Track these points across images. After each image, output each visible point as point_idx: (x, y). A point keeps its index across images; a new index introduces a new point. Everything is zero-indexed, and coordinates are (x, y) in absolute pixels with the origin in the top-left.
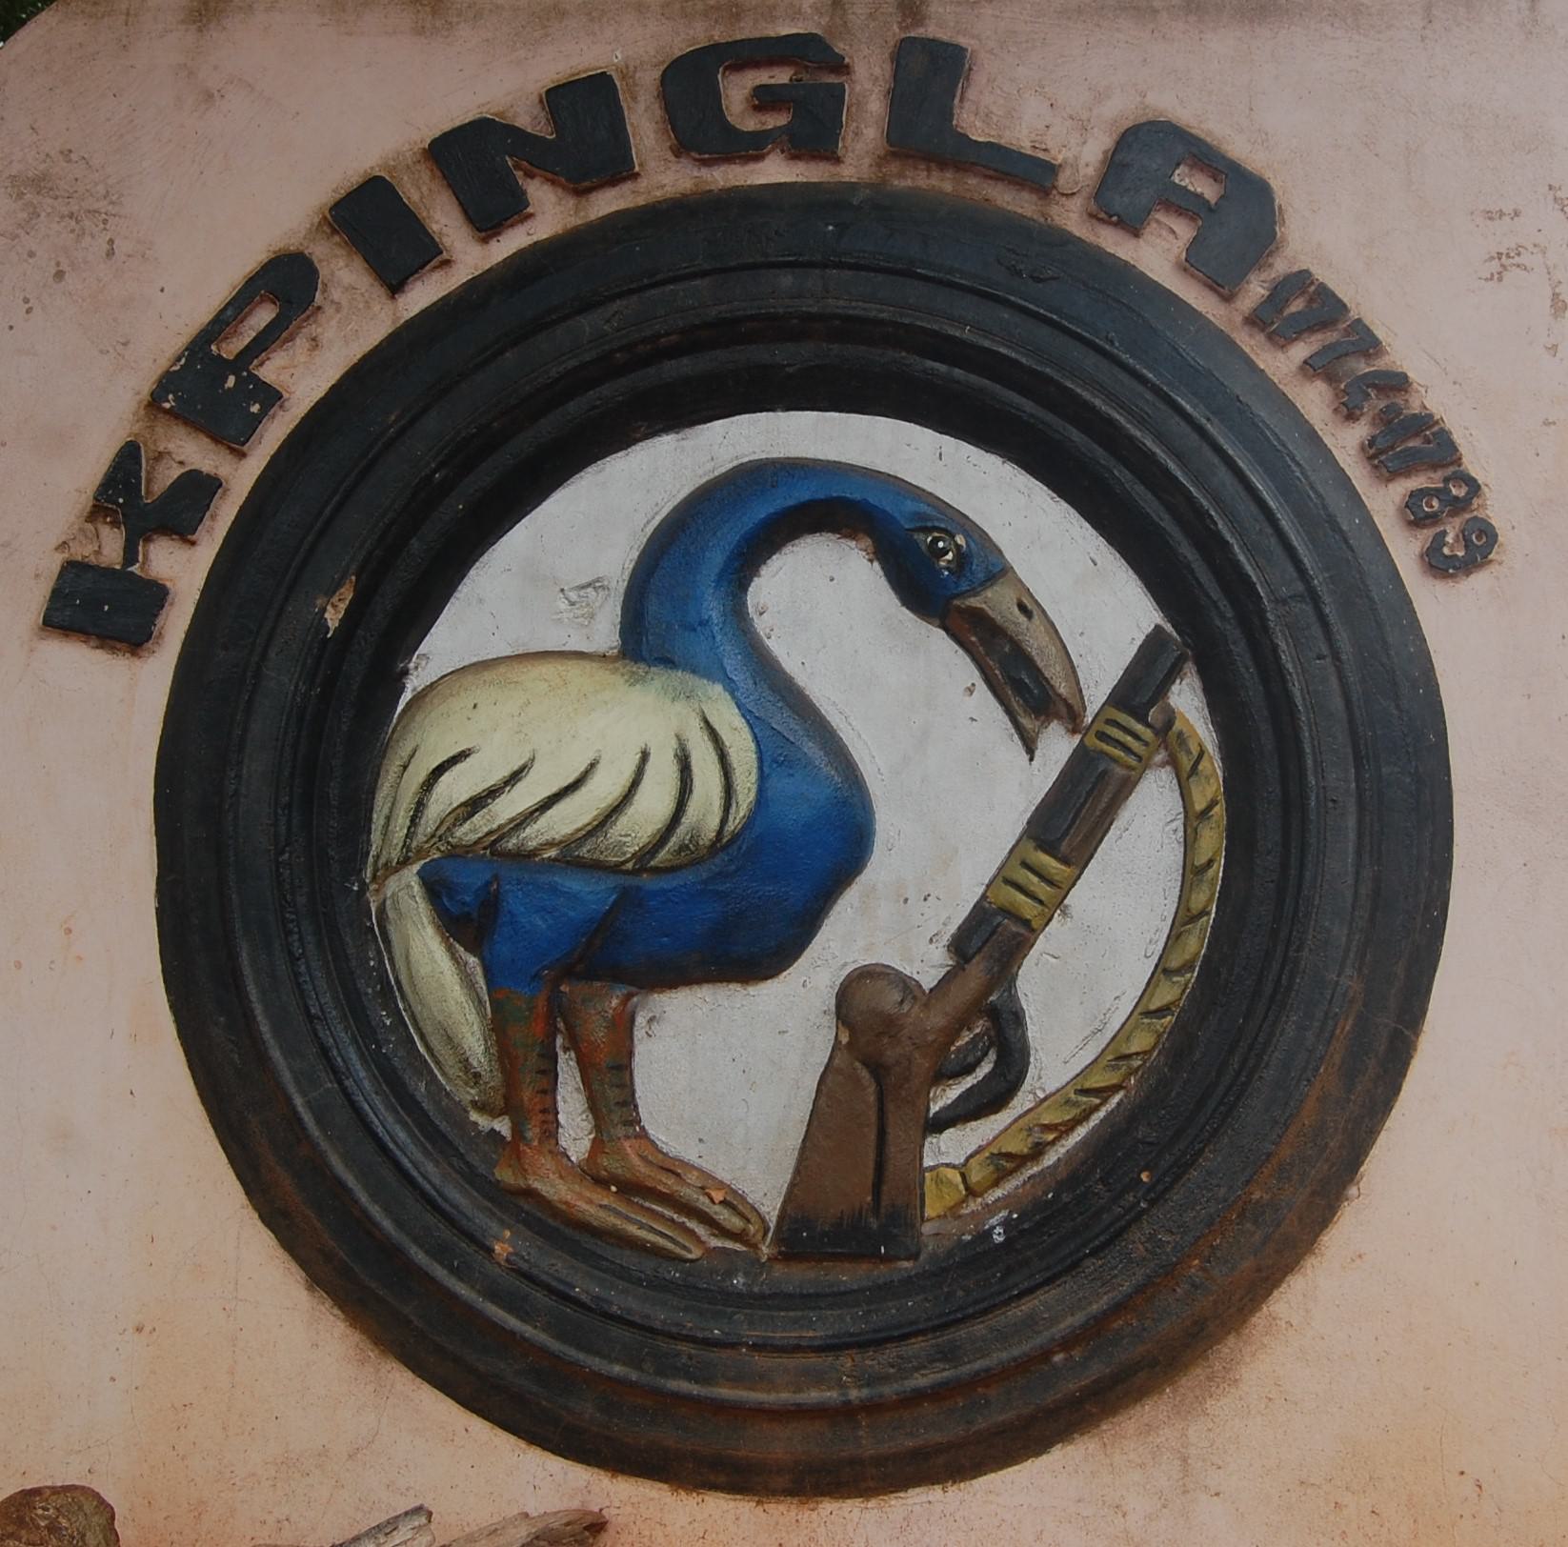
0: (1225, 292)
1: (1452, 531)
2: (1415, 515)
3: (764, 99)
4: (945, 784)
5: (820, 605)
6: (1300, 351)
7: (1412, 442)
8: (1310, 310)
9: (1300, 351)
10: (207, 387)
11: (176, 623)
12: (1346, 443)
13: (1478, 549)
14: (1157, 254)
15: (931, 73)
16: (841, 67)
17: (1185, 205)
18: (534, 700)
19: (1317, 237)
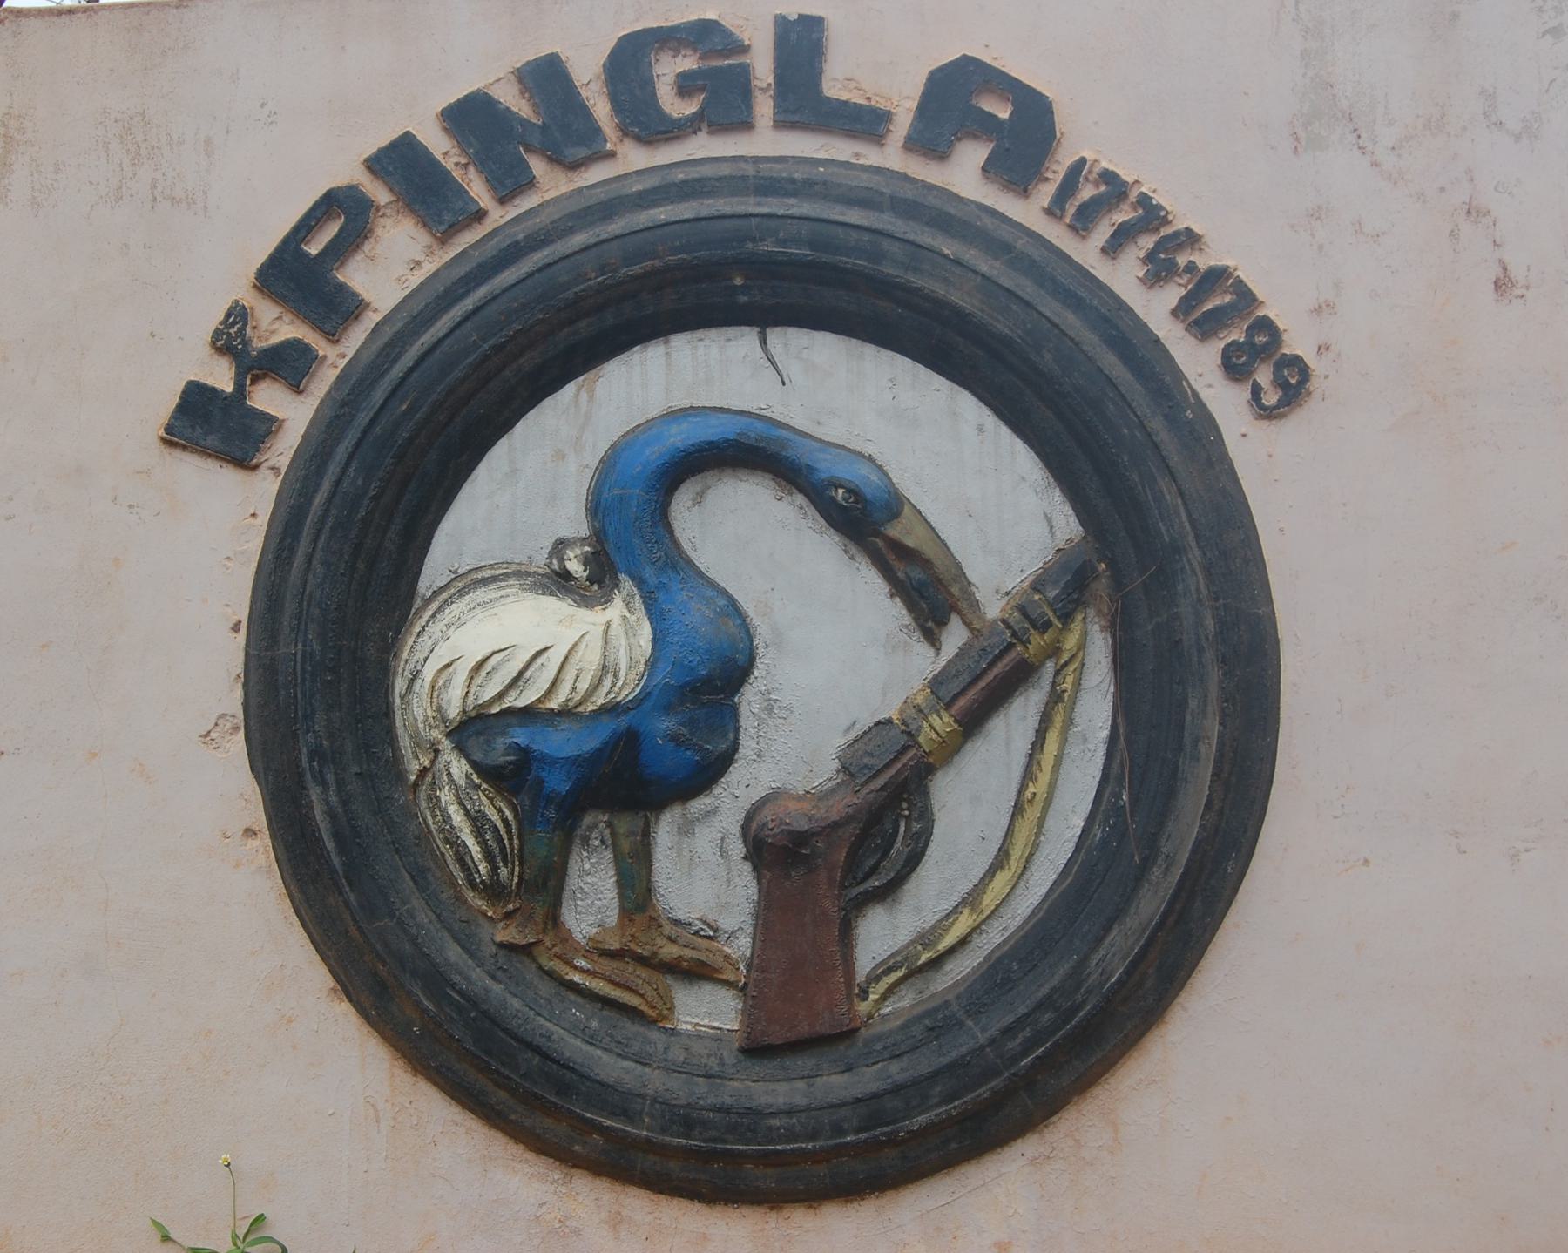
0: (328, 328)
1: (1264, 376)
2: (1235, 366)
3: (685, 85)
4: (830, 666)
5: (741, 536)
6: (1102, 233)
7: (1217, 302)
8: (1102, 198)
9: (1102, 233)
10: (302, 275)
11: (283, 450)
12: (1156, 309)
13: (1294, 384)
14: (964, 174)
15: (801, 43)
16: (744, 49)
17: (985, 126)
18: (508, 632)
19: (1089, 135)
